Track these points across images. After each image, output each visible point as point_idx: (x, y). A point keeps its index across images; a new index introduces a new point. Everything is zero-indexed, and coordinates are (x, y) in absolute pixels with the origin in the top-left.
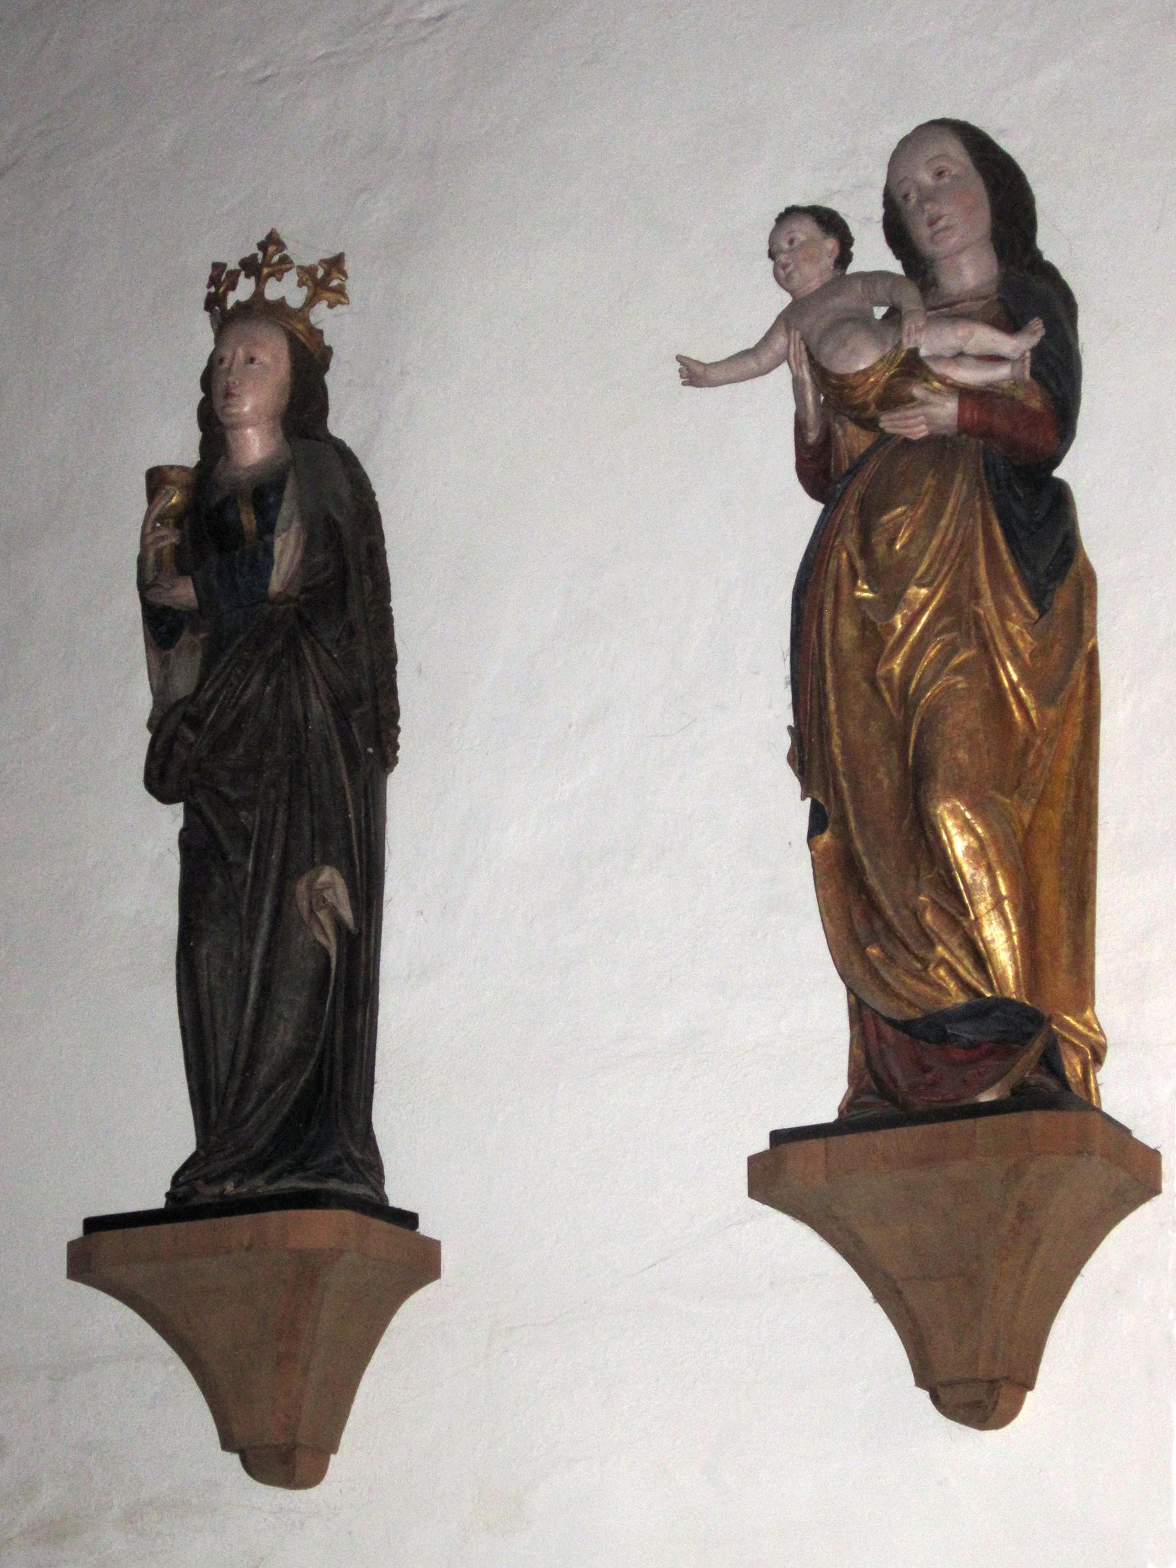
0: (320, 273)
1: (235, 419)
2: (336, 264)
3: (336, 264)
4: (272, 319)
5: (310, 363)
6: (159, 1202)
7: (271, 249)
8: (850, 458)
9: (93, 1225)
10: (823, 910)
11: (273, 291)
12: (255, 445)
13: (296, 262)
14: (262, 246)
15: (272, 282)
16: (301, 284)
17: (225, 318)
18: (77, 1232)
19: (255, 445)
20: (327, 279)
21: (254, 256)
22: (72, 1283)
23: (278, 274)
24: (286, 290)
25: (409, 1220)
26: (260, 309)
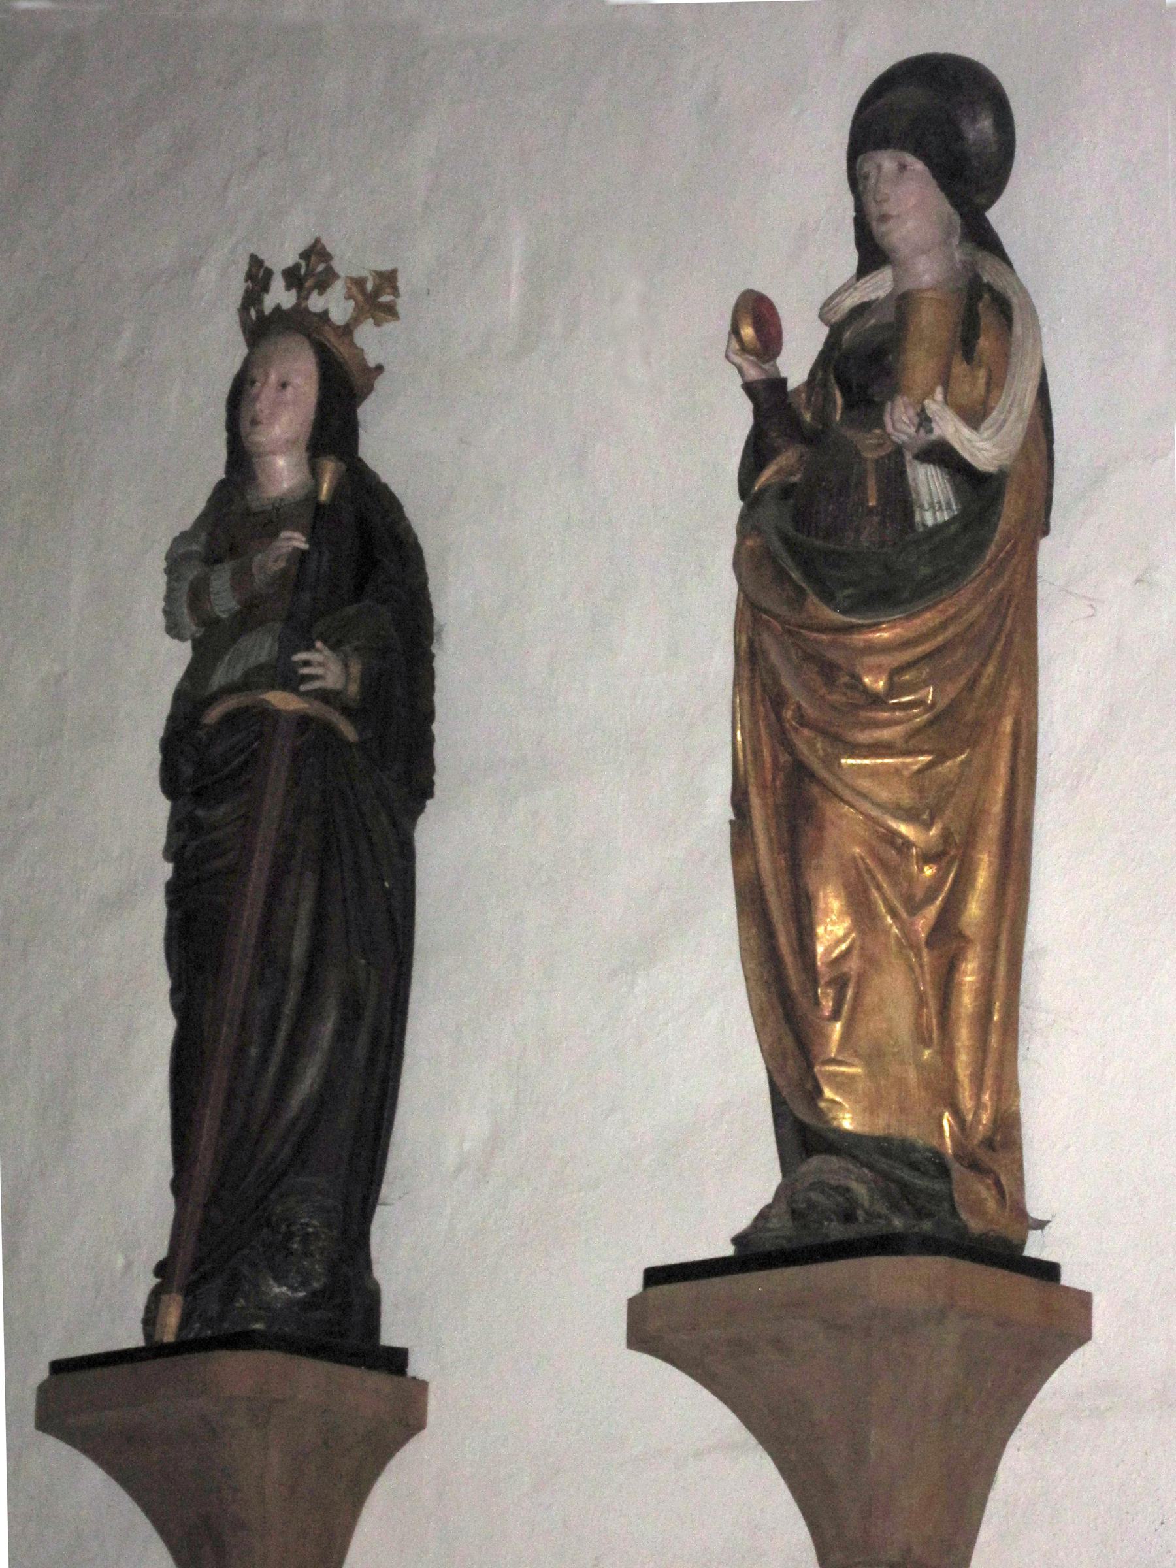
0: (369, 286)
1: (261, 450)
2: (388, 279)
3: (388, 279)
4: (313, 337)
5: (342, 392)
6: (727, 1250)
7: (313, 259)
8: (346, 711)
9: (655, 1276)
10: (385, 1124)
11: (316, 303)
12: (283, 473)
13: (342, 274)
14: (306, 255)
15: (314, 295)
16: (349, 297)
17: (260, 329)
18: (635, 1285)
19: (283, 473)
20: (378, 297)
21: (297, 267)
22: (1086, 1288)
23: (323, 285)
24: (335, 304)
25: (1049, 1271)
26: (302, 324)
